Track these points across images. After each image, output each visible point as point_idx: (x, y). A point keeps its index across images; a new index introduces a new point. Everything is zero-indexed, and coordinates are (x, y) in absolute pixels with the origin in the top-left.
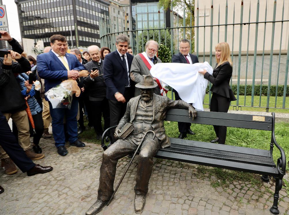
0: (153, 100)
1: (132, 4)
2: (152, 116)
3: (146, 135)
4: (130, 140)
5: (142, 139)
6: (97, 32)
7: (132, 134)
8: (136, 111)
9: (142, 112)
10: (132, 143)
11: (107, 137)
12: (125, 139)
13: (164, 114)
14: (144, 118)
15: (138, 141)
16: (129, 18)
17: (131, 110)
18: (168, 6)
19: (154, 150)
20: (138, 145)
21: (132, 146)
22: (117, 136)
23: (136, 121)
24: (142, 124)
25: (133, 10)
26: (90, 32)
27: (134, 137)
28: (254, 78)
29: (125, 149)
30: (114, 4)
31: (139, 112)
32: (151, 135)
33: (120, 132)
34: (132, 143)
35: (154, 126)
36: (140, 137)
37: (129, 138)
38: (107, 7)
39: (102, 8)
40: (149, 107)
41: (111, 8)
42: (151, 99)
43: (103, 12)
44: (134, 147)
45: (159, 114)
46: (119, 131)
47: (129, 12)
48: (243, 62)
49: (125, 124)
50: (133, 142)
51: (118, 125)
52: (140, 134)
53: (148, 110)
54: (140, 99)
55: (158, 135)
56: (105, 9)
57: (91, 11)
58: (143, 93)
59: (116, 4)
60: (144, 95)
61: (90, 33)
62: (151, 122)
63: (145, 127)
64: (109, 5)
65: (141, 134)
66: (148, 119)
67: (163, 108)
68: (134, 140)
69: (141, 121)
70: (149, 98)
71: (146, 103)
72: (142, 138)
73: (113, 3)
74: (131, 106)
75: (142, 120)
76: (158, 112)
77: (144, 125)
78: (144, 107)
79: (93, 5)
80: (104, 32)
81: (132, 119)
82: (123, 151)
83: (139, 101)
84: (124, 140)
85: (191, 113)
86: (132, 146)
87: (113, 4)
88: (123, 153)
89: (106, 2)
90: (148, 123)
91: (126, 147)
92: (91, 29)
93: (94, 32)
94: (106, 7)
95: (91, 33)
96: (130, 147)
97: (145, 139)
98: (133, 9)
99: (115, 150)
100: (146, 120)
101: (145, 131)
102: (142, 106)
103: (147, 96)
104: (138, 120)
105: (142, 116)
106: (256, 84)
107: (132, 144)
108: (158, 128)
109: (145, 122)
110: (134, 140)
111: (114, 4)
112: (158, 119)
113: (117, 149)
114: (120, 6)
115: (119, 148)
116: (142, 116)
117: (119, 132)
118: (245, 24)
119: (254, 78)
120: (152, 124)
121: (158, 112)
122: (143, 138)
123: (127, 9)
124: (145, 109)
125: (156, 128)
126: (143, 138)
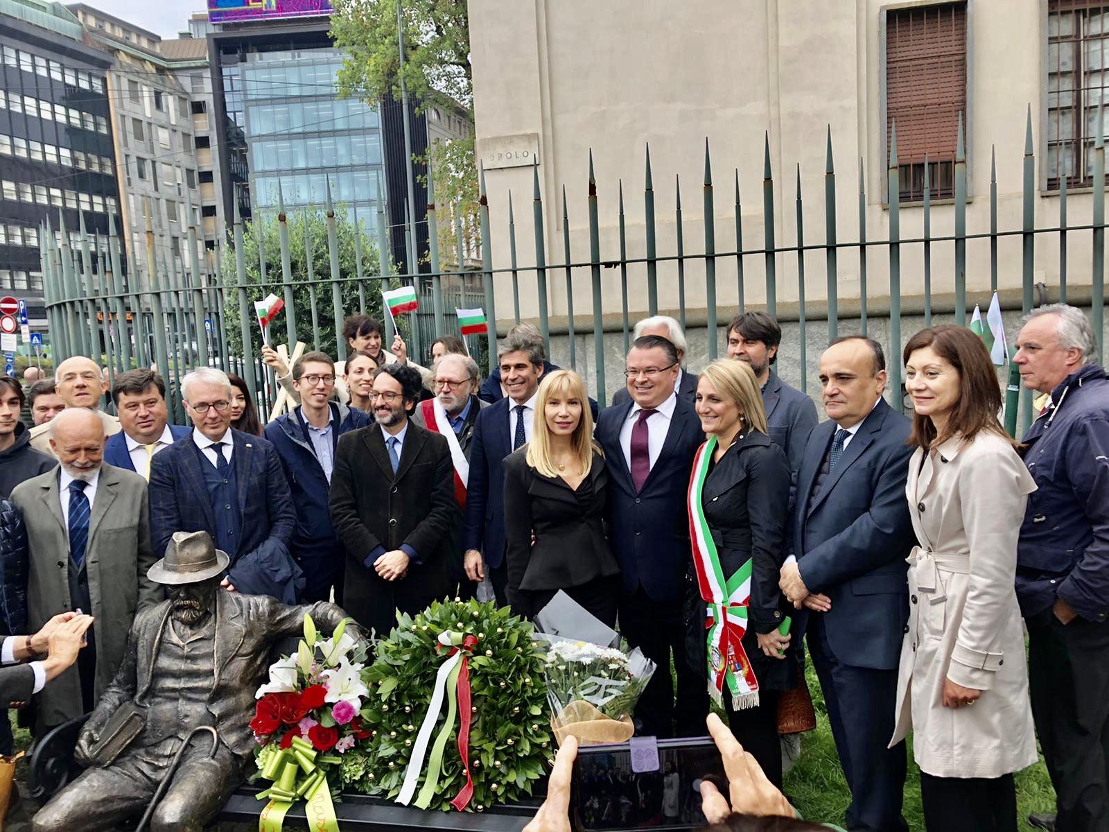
1: (224, 57)
2: (211, 673)
3: (189, 745)
4: (129, 765)
5: (175, 760)
6: (50, 197)
7: (137, 742)
8: (156, 659)
9: (177, 662)
11: (51, 761)
13: (259, 662)
14: (182, 684)
15: (161, 768)
16: (205, 125)
17: (140, 655)
18: (383, 84)
19: (205, 797)
21: (137, 788)
22: (85, 756)
23: (154, 696)
24: (174, 704)
25: (227, 87)
26: (15, 198)
27: (148, 753)
30: (133, 57)
31: (165, 662)
32: (206, 741)
33: (97, 742)
34: (138, 775)
36: (167, 752)
37: (127, 758)
38: (97, 77)
39: (70, 80)
40: (199, 644)
41: (119, 77)
42: (207, 615)
43: (74, 98)
44: (147, 788)
45: (241, 663)
46: (91, 735)
47: (206, 94)
48: (695, 354)
49: (120, 705)
50: (143, 773)
51: (94, 713)
54: (170, 614)
55: (231, 739)
56: (84, 85)
57: (18, 99)
58: (177, 597)
59: (144, 60)
60: (177, 603)
61: (11, 202)
62: (206, 696)
63: (186, 716)
64: (105, 65)
65: (172, 741)
66: (196, 685)
68: (147, 763)
69: (173, 695)
70: (199, 611)
71: (191, 628)
72: (174, 754)
73: (126, 54)
74: (140, 641)
75: (174, 690)
76: (233, 657)
78: (181, 643)
79: (27, 67)
80: (63, 290)
81: (142, 688)
82: (101, 809)
83: (166, 623)
84: (106, 768)
86: (137, 788)
87: (128, 61)
88: (101, 813)
89: (91, 53)
90: (197, 701)
91: (114, 793)
92: (16, 183)
93: (34, 198)
94: (90, 75)
95: (21, 204)
96: (131, 791)
97: (183, 756)
98: (227, 83)
100: (190, 690)
101: (185, 729)
102: (175, 639)
103: (191, 607)
104: (163, 690)
105: (176, 675)
107: (135, 780)
108: (233, 715)
110: (147, 763)
111: (133, 57)
112: (236, 683)
114: (161, 70)
115: (88, 797)
116: (176, 675)
117: (92, 742)
118: (608, 265)
120: (211, 701)
121: (233, 657)
122: (177, 755)
123: (197, 79)
124: (187, 649)
125: (223, 717)
126: (177, 755)
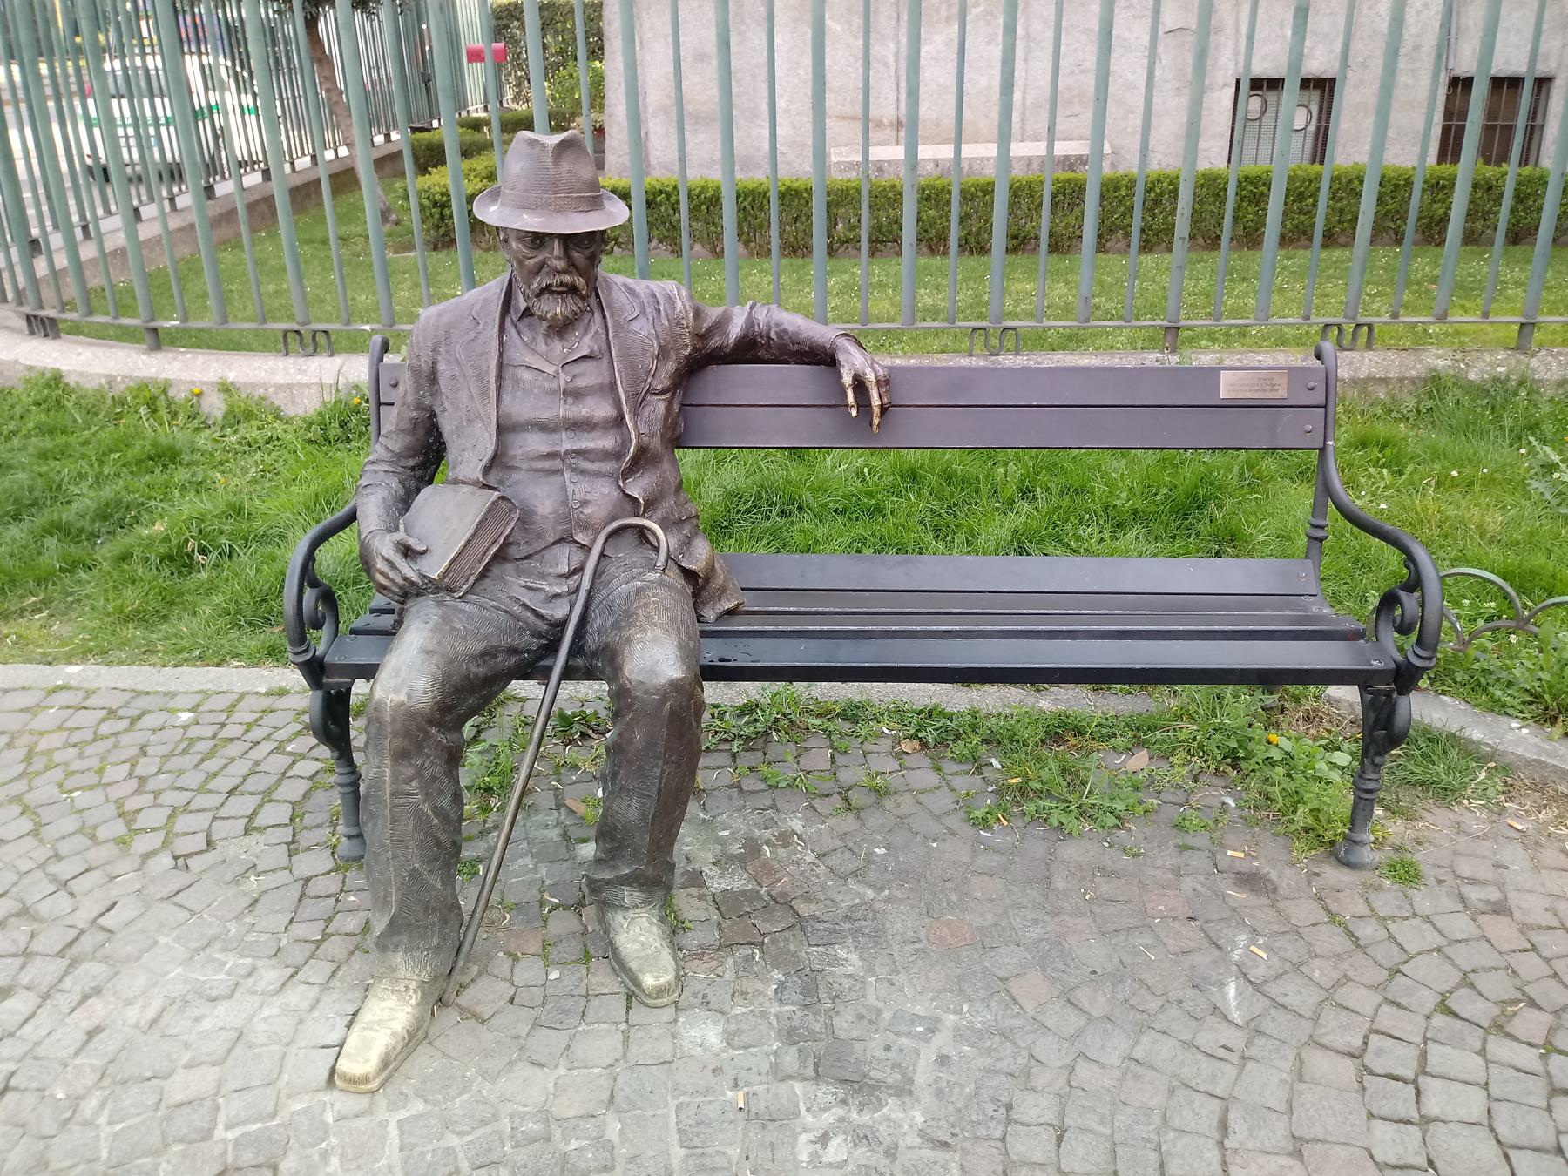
0: (604, 317)
10: (516, 608)
12: (470, 591)
20: (563, 624)
27: (520, 573)
28: (1004, 137)
29: (487, 654)
31: (521, 408)
34: (516, 608)
35: (637, 488)
52: (556, 549)
53: (581, 383)
63: (585, 503)
67: (671, 366)
69: (547, 464)
77: (579, 488)
78: (551, 369)
85: (859, 384)
99: (442, 665)
100: (580, 453)
105: (543, 428)
106: (1018, 172)
109: (574, 470)
112: (656, 444)
113: (452, 661)
119: (1004, 137)
120: (628, 472)
124: (563, 378)
125: (651, 504)
